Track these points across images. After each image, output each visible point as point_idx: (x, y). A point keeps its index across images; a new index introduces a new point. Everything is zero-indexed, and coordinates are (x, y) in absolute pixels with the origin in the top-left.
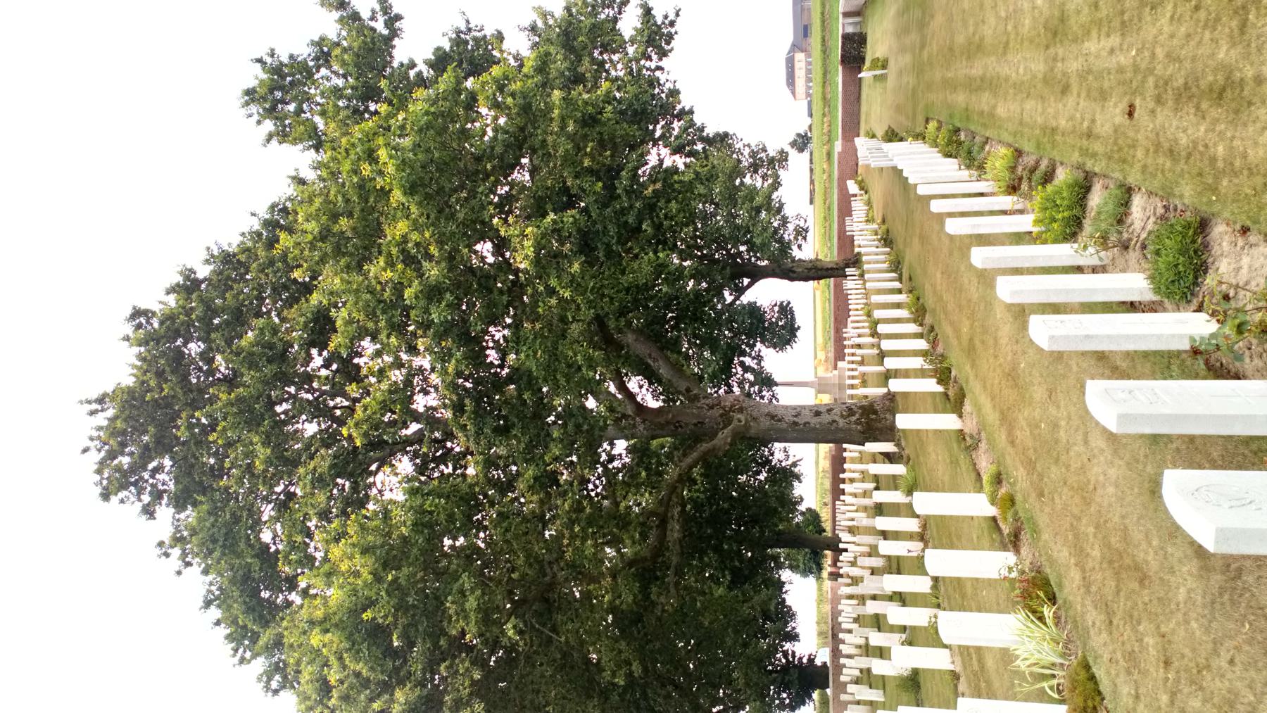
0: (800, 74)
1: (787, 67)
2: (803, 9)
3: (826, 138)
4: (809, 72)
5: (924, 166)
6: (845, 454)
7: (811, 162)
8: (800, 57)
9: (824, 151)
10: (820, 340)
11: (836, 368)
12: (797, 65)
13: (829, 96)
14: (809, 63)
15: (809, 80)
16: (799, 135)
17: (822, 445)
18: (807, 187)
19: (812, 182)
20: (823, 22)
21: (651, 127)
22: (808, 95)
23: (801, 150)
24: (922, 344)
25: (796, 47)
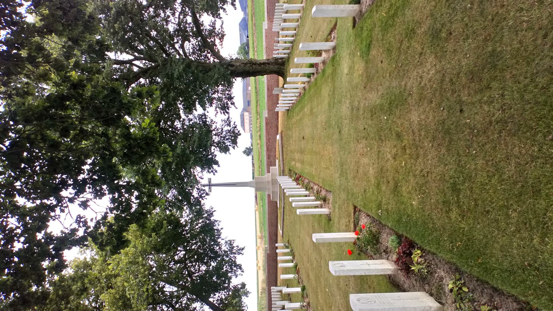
0: (247, 121)
1: (241, 118)
2: (247, 94)
3: (258, 129)
4: (250, 121)
5: (286, 182)
6: (277, 251)
7: (253, 159)
8: (246, 114)
9: (258, 135)
10: (261, 264)
11: (269, 172)
12: (245, 117)
13: (259, 111)
14: (251, 117)
15: (250, 124)
16: (247, 148)
17: (259, 77)
18: (255, 262)
19: (253, 164)
20: (257, 102)
21: (43, 240)
22: (250, 131)
23: (248, 155)
24: (290, 258)
25: (244, 110)
